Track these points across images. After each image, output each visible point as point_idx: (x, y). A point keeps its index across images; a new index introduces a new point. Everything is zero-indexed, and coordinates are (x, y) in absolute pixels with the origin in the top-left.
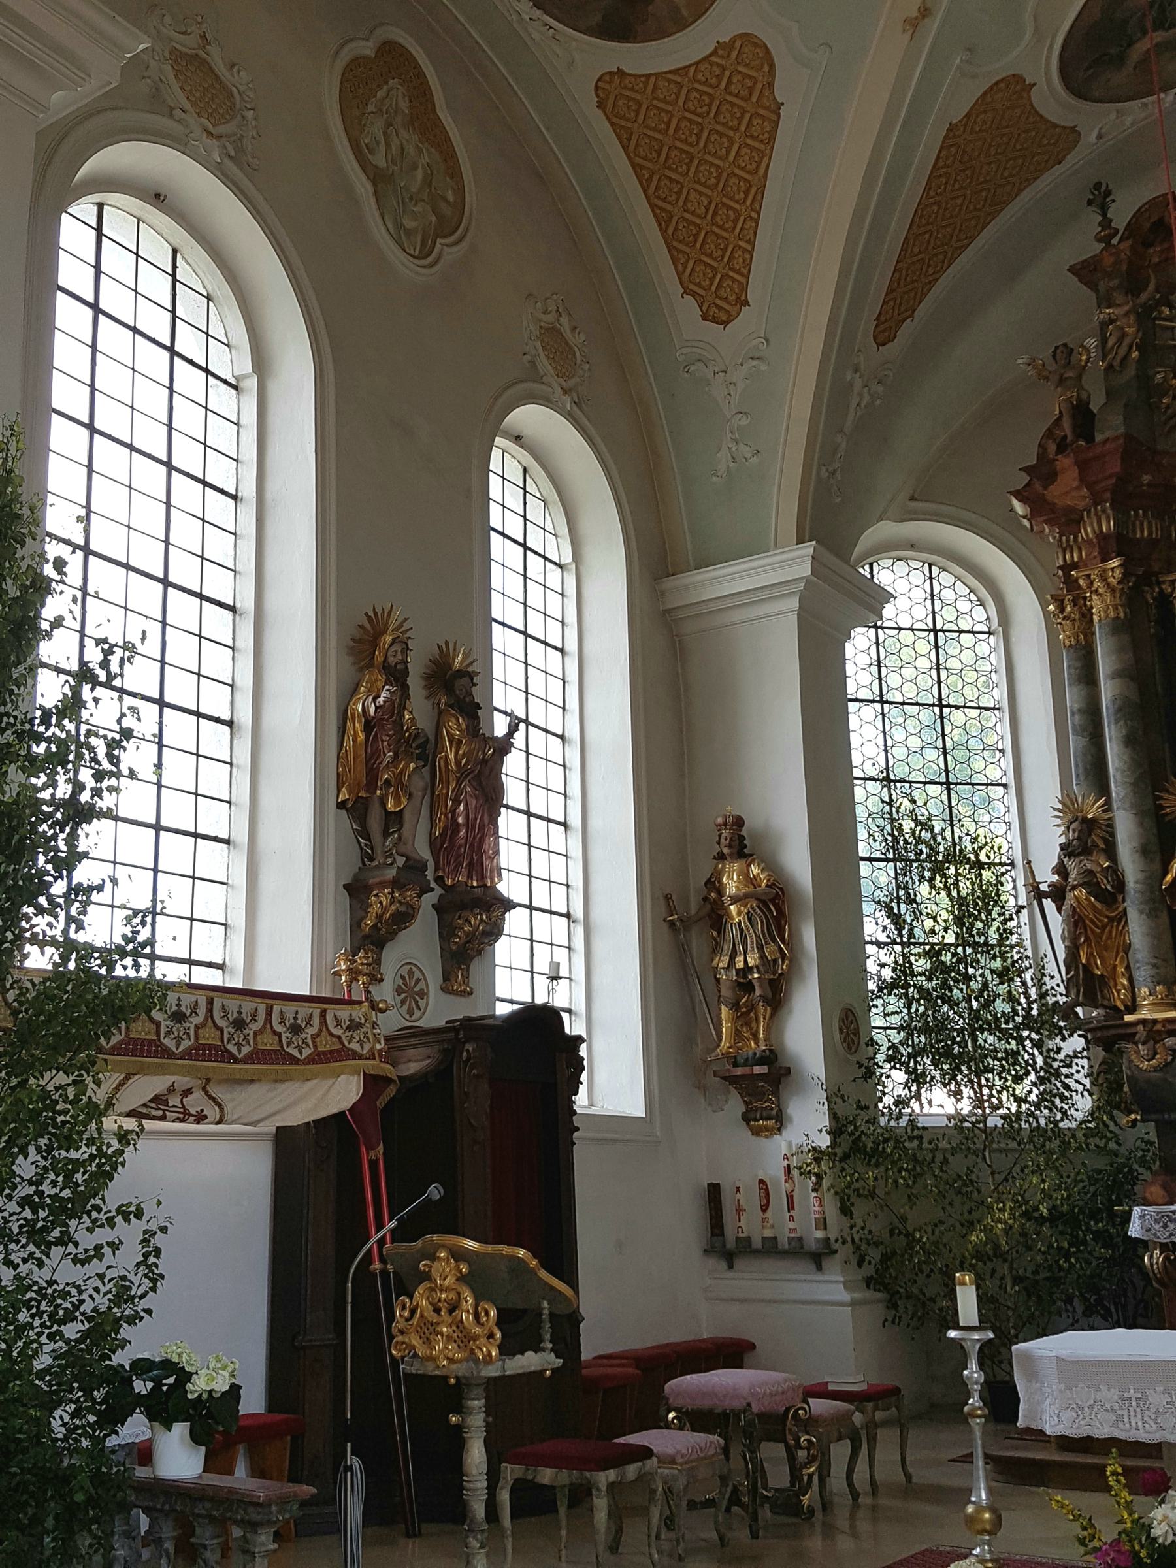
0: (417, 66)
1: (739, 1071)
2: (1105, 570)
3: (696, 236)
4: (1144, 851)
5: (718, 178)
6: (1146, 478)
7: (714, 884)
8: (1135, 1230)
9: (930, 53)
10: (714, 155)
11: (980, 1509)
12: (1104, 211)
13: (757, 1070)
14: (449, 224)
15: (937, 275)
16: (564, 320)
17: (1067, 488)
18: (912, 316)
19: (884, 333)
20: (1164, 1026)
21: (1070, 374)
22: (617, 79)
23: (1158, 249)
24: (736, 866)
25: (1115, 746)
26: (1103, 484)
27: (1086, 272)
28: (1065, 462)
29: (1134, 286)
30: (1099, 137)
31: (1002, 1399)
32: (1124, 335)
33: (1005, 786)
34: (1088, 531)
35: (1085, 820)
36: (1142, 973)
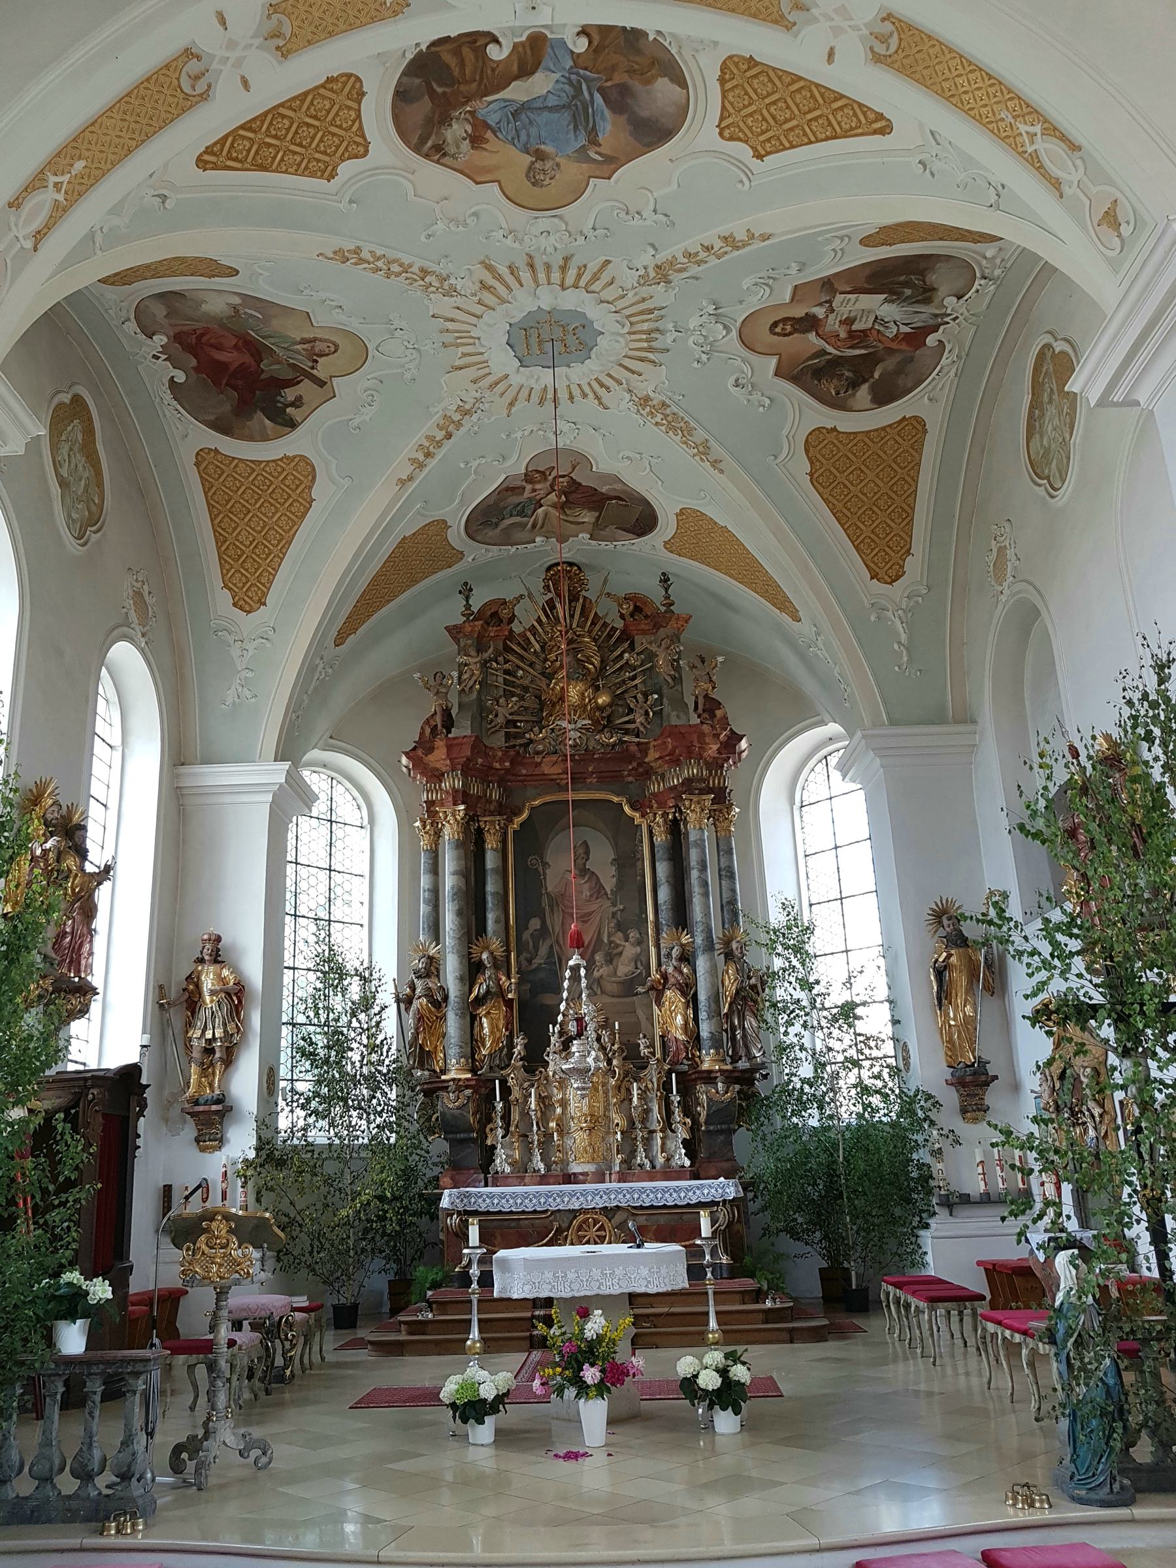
0: (89, 412)
1: (201, 1108)
3: (240, 556)
4: (461, 979)
5: (263, 528)
6: (480, 761)
7: (193, 980)
8: (445, 1203)
10: (264, 514)
11: (474, 1342)
12: (467, 598)
13: (214, 1108)
17: (438, 757)
22: (212, 454)
24: (211, 968)
31: (486, 1280)
34: (446, 785)
35: (429, 957)
36: (453, 1051)
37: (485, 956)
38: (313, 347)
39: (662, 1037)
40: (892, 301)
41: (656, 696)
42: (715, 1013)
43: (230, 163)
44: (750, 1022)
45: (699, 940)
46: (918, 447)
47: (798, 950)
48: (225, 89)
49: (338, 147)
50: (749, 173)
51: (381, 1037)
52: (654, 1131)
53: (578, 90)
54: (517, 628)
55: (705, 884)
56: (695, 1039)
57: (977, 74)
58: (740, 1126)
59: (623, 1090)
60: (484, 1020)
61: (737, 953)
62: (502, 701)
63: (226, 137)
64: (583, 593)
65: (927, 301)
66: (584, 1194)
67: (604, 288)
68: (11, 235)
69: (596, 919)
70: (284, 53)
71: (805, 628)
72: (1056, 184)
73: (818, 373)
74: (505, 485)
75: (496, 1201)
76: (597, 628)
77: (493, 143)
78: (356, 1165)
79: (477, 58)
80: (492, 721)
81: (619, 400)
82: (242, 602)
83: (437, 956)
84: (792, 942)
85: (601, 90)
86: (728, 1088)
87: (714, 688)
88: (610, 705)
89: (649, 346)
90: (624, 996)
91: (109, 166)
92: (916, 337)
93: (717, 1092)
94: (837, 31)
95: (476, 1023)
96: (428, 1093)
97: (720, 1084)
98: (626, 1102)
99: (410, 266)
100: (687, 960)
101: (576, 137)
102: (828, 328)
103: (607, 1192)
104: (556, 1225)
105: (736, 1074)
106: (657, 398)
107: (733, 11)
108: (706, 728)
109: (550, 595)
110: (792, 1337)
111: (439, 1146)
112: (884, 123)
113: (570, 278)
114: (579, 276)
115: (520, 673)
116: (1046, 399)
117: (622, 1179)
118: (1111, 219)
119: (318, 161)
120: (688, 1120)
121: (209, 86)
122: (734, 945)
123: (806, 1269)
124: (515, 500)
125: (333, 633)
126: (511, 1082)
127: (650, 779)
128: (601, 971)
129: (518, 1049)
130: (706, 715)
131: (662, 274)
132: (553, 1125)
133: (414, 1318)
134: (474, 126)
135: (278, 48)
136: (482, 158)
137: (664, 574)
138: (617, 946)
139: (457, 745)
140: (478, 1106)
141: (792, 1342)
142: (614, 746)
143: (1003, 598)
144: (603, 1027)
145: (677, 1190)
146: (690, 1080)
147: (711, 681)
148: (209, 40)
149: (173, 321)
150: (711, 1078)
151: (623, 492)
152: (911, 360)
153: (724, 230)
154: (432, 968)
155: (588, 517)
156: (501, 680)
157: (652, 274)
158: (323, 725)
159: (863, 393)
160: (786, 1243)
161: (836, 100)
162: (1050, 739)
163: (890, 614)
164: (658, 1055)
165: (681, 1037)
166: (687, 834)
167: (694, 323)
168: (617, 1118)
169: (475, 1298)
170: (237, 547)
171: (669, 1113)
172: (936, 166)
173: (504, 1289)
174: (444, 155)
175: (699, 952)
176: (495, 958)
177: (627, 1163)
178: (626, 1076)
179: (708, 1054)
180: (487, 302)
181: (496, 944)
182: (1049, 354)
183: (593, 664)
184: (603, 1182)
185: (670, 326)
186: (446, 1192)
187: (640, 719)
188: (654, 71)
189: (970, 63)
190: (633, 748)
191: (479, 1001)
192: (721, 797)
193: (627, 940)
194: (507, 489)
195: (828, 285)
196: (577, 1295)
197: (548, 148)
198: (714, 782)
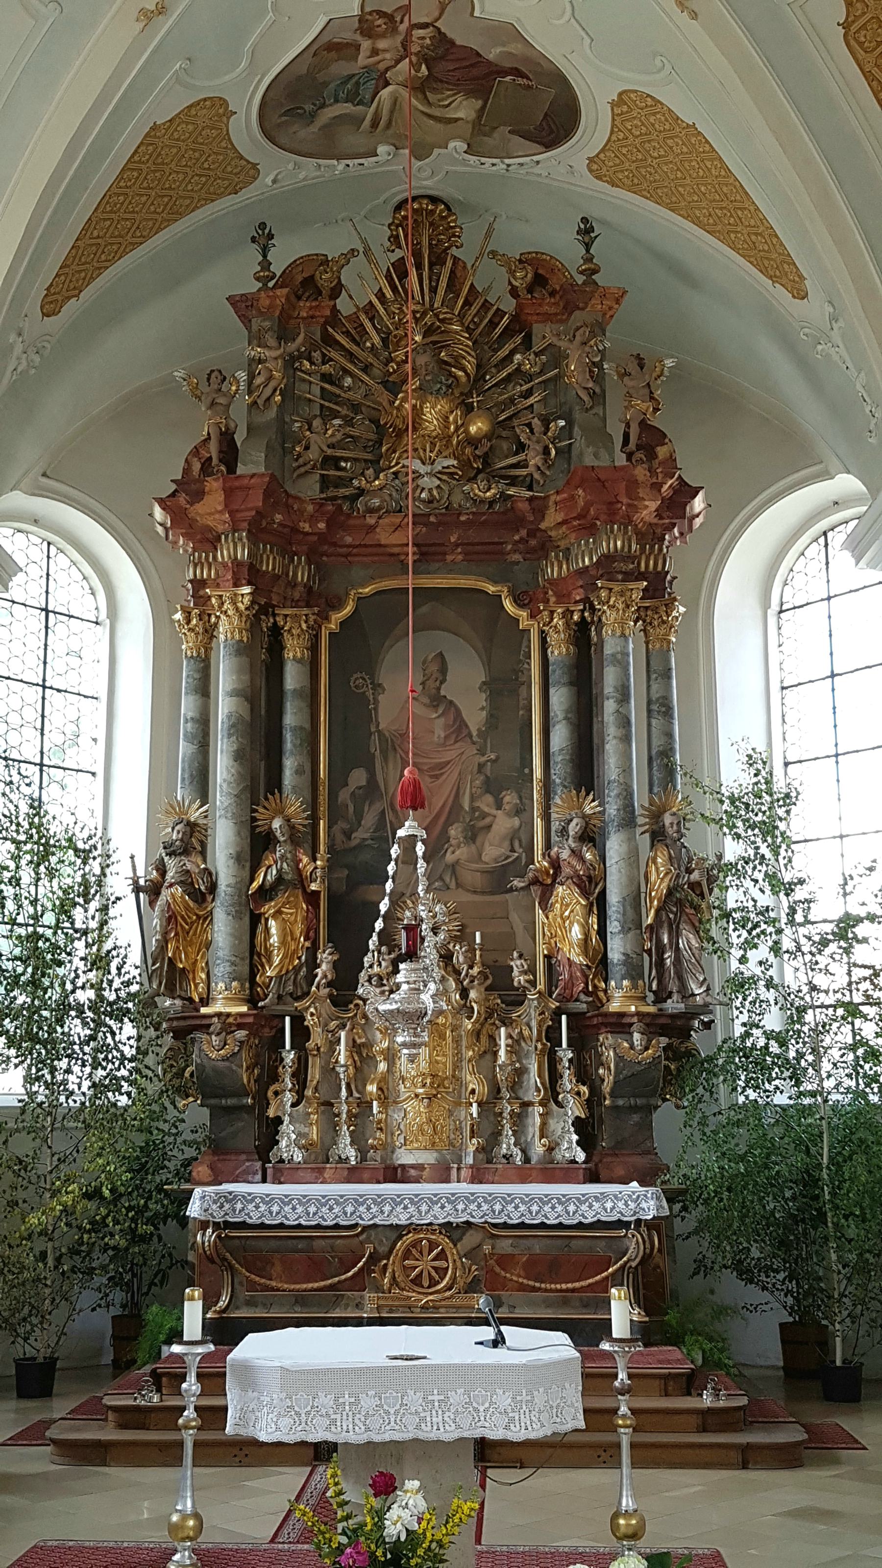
2: (235, 595)
4: (238, 858)
8: (194, 1210)
9: (154, 52)
15: (108, 264)
17: (211, 508)
18: (77, 296)
19: (51, 305)
20: (235, 1019)
23: (308, 304)
25: (225, 758)
26: (242, 514)
27: (243, 305)
28: (214, 485)
29: (284, 335)
30: (274, 181)
32: (270, 378)
33: (94, 774)
34: (224, 554)
35: (189, 823)
36: (221, 970)
37: (276, 824)
39: (548, 957)
41: (562, 423)
42: (633, 923)
44: (688, 939)
45: (612, 809)
47: (768, 829)
51: (108, 945)
52: (529, 1104)
54: (344, 306)
55: (625, 723)
56: (601, 963)
58: (665, 1100)
59: (484, 1039)
60: (272, 923)
61: (671, 831)
62: (317, 423)
64: (454, 251)
66: (416, 1200)
69: (450, 778)
71: (812, 310)
74: (325, 38)
75: (275, 1208)
76: (474, 310)
78: (61, 1144)
80: (299, 455)
83: (200, 822)
84: (760, 818)
86: (649, 1041)
87: (656, 410)
88: (489, 436)
90: (492, 893)
93: (632, 1047)
95: (260, 928)
96: (179, 1034)
97: (637, 1036)
98: (488, 1057)
100: (592, 840)
103: (453, 1199)
104: (369, 1249)
105: (663, 1021)
108: (640, 472)
109: (399, 254)
110: (747, 1458)
111: (195, 1114)
117: (477, 1178)
120: (584, 1089)
122: (668, 819)
123: (759, 1331)
124: (342, 68)
125: (37, 293)
126: (309, 1021)
127: (546, 559)
128: (457, 853)
129: (324, 969)
132: (372, 1088)
133: (131, 1402)
137: (585, 220)
138: (484, 815)
139: (240, 488)
140: (257, 1055)
141: (745, 1466)
142: (492, 503)
144: (456, 939)
145: (563, 1201)
146: (588, 1026)
147: (652, 398)
150: (624, 1025)
151: (527, 60)
154: (192, 840)
155: (464, 109)
156: (317, 390)
160: (730, 1288)
164: (541, 986)
165: (579, 959)
166: (601, 642)
168: (472, 1082)
169: (189, 1437)
171: (554, 1077)
173: (243, 1419)
175: (611, 829)
176: (292, 827)
177: (487, 1151)
178: (490, 1016)
179: (619, 987)
181: (295, 805)
183: (463, 369)
184: (447, 1181)
186: (198, 1191)
187: (535, 460)
190: (523, 506)
191: (265, 893)
192: (658, 589)
193: (499, 807)
194: (329, 48)
196: (377, 1438)
198: (646, 564)
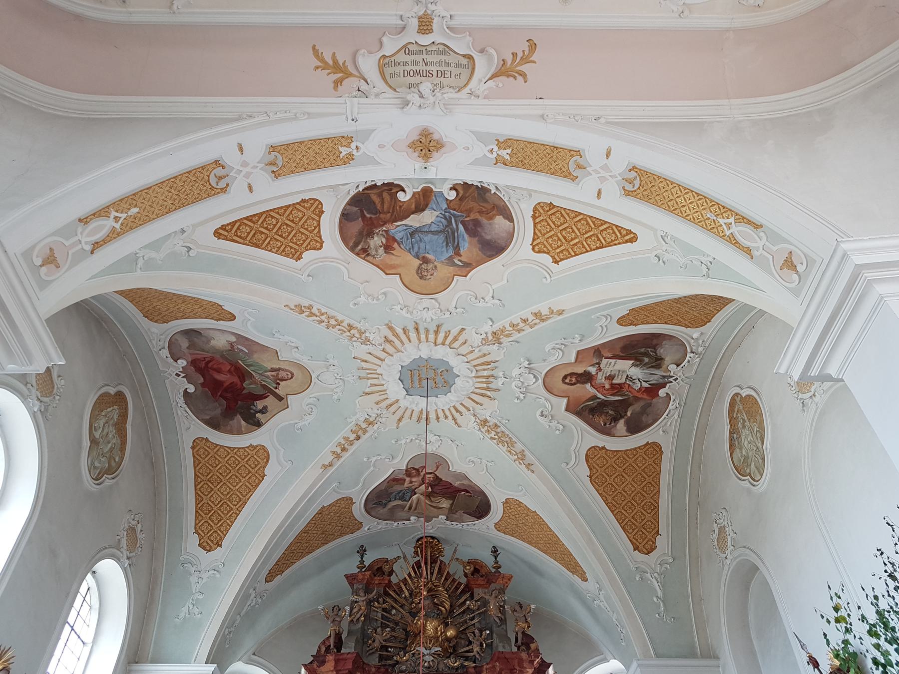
0: (127, 405)
3: (210, 511)
14: (111, 470)
16: (140, 526)
19: (269, 578)
21: (338, 619)
29: (367, 591)
32: (360, 609)
38: (278, 374)
40: (637, 366)
43: (235, 238)
46: (658, 462)
48: (238, 187)
49: (304, 241)
50: (550, 273)
53: (450, 222)
54: (394, 579)
57: (690, 194)
62: (379, 630)
63: (236, 222)
64: (441, 558)
65: (658, 367)
67: (460, 346)
68: (76, 238)
70: (276, 175)
71: (591, 586)
72: (748, 251)
73: (593, 411)
74: (392, 477)
76: (449, 582)
77: (397, 250)
79: (391, 199)
81: (468, 422)
82: (205, 544)
85: (463, 223)
87: (529, 627)
88: (456, 637)
89: (487, 388)
91: (154, 216)
92: (652, 390)
94: (603, 179)
99: (342, 322)
101: (447, 250)
102: (598, 382)
106: (492, 421)
107: (541, 171)
108: (524, 655)
109: (418, 558)
112: (632, 236)
113: (440, 339)
114: (446, 337)
115: (394, 611)
116: (740, 426)
118: (789, 264)
119: (292, 248)
121: (228, 185)
124: (398, 488)
125: (265, 572)
130: (523, 647)
131: (497, 337)
134: (387, 240)
135: (273, 172)
136: (392, 260)
137: (494, 547)
139: (342, 659)
143: (728, 562)
148: (231, 158)
149: (191, 351)
151: (470, 486)
152: (650, 405)
153: (535, 309)
155: (445, 504)
157: (490, 338)
158: (249, 643)
159: (621, 425)
161: (602, 225)
162: (840, 593)
163: (649, 575)
167: (515, 372)
170: (209, 505)
172: (666, 257)
174: (368, 255)
180: (388, 350)
182: (738, 399)
185: (501, 374)
187: (476, 649)
188: (494, 212)
189: (685, 189)
194: (394, 480)
195: (598, 352)
197: (430, 256)
